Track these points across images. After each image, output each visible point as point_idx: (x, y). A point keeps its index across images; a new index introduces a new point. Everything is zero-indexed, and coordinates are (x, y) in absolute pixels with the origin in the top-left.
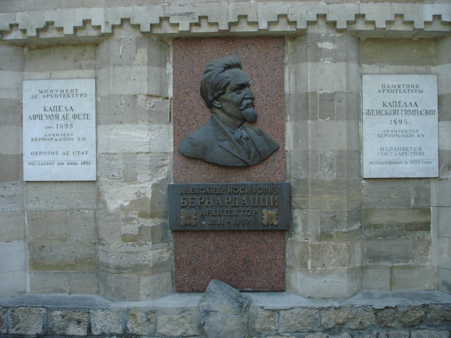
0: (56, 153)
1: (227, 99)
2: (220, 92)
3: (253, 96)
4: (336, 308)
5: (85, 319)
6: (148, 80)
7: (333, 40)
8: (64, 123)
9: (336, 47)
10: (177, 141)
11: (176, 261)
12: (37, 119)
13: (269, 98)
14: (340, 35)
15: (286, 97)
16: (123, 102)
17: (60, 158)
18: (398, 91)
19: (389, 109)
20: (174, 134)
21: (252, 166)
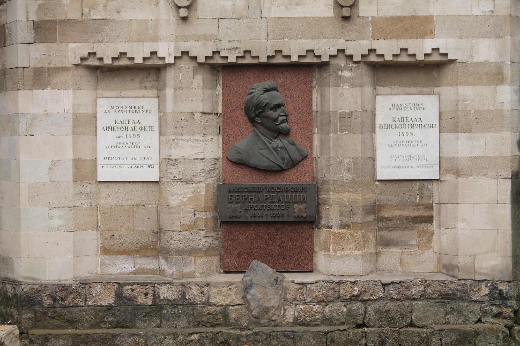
0: (125, 158)
1: (266, 100)
2: (260, 111)
3: (287, 113)
4: (351, 283)
5: (151, 292)
6: (203, 100)
7: (351, 70)
8: (132, 133)
9: (353, 75)
10: (225, 149)
11: (224, 247)
12: (110, 130)
13: (300, 115)
14: (356, 65)
15: (314, 114)
16: (183, 118)
17: (129, 162)
18: (405, 109)
19: (398, 123)
20: (223, 143)
21: (286, 170)
